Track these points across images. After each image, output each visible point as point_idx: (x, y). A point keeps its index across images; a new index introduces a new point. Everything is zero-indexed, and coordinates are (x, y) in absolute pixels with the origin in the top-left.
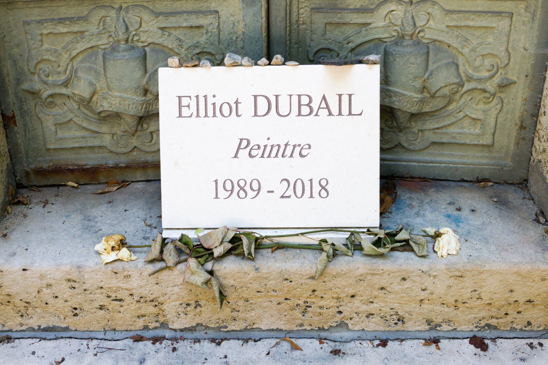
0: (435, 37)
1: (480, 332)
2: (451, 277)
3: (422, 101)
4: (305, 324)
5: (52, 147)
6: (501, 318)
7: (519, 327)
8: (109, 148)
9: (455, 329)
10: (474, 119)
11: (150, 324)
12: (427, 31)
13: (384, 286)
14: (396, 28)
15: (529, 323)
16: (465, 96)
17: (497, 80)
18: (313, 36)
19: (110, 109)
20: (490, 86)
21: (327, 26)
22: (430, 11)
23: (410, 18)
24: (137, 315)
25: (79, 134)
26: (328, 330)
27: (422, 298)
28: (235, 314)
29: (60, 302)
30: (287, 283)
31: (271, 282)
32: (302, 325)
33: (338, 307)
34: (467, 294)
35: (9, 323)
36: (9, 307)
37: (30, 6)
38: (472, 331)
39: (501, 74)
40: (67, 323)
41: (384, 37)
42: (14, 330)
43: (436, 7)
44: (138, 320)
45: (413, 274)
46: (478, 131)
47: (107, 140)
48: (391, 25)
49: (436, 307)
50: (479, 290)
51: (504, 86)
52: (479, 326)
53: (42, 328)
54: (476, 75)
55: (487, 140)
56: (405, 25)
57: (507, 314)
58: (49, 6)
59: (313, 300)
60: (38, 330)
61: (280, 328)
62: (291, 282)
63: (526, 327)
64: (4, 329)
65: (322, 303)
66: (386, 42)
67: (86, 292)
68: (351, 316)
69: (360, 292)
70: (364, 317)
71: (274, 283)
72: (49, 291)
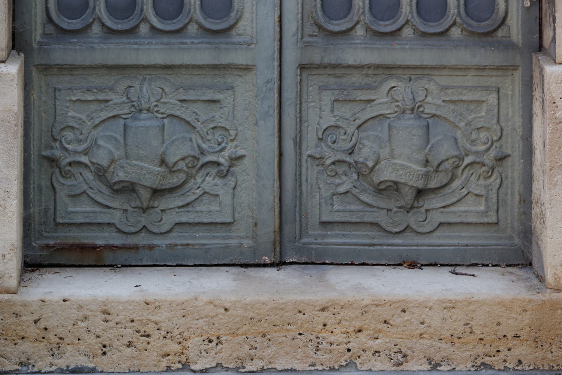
0: (434, 112)
1: (477, 372)
2: (444, 308)
3: (427, 175)
4: (317, 364)
5: (62, 221)
6: (494, 356)
7: (511, 366)
8: (118, 226)
9: (454, 369)
10: (477, 195)
11: (173, 365)
12: (426, 106)
13: (387, 318)
14: (398, 104)
15: (520, 362)
16: (466, 171)
17: (493, 153)
18: (322, 113)
19: (126, 179)
20: (489, 159)
21: (335, 104)
22: (427, 86)
23: (410, 93)
24: (162, 353)
25: (90, 208)
26: (338, 370)
27: (422, 332)
28: (252, 352)
29: (92, 338)
30: (300, 315)
31: (286, 314)
32: (314, 365)
33: (346, 344)
34: (460, 327)
35: (40, 363)
36: (43, 344)
37: (63, 73)
38: (469, 370)
39: (496, 147)
40: (95, 363)
41: (388, 112)
42: (43, 371)
43: (432, 83)
44: (162, 359)
45: (411, 305)
46: (482, 208)
47: (116, 217)
48: (393, 101)
49: (434, 343)
50: (471, 323)
51: (501, 159)
52: (476, 365)
53: (70, 368)
54: (474, 149)
55: (494, 219)
56: (406, 99)
57: (499, 351)
58: (80, 74)
59: (324, 335)
60: (67, 370)
61: (294, 368)
62: (304, 314)
63: (517, 366)
64: (33, 371)
65: (332, 338)
66: (389, 118)
67: (119, 326)
68: (359, 354)
69: (366, 326)
70: (371, 355)
71: (290, 314)
72: (83, 324)
